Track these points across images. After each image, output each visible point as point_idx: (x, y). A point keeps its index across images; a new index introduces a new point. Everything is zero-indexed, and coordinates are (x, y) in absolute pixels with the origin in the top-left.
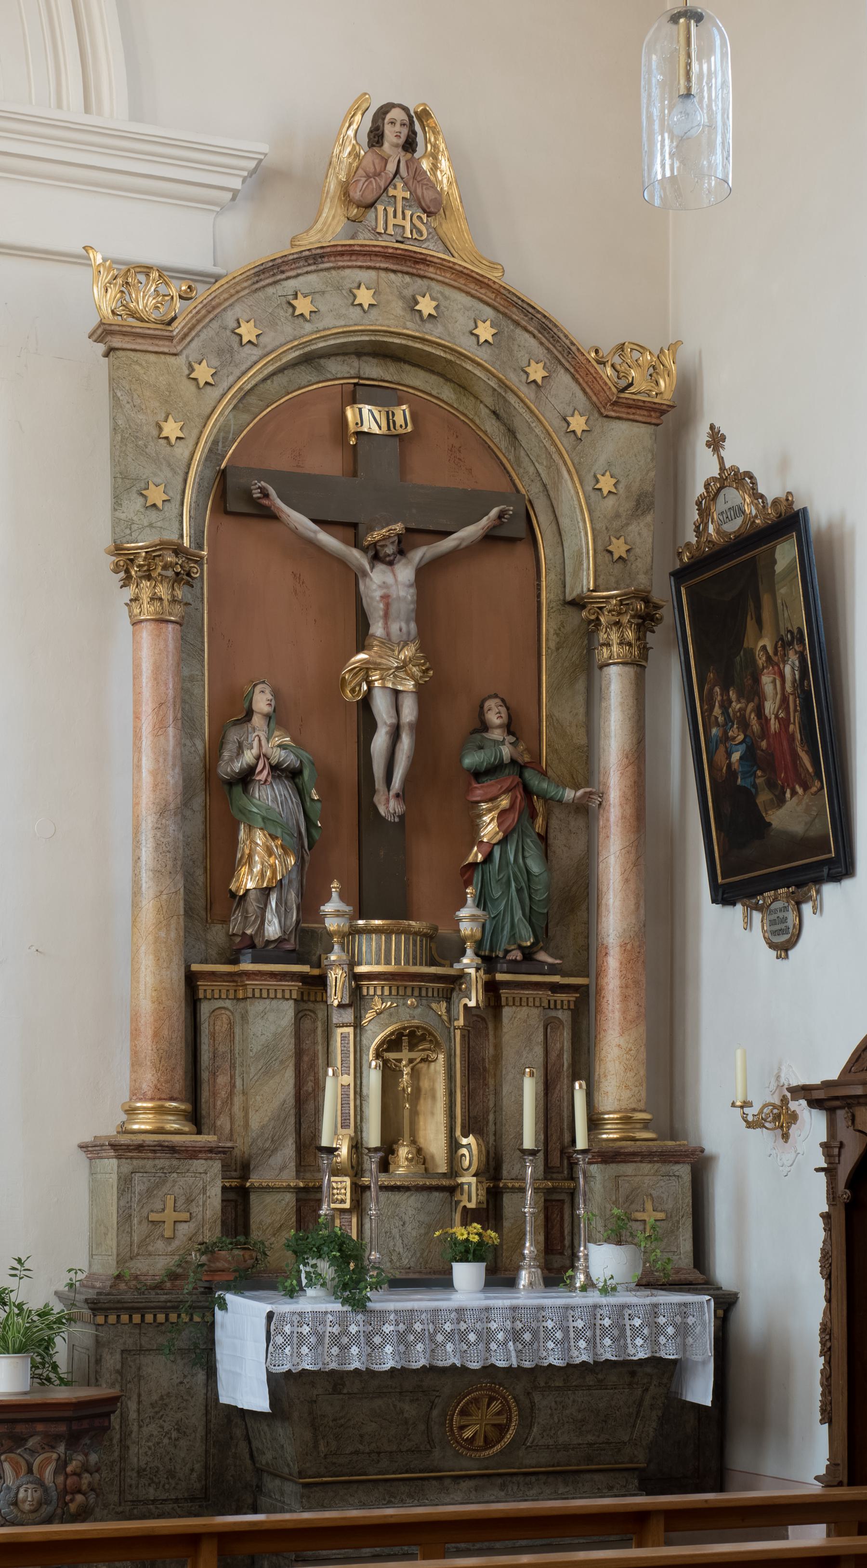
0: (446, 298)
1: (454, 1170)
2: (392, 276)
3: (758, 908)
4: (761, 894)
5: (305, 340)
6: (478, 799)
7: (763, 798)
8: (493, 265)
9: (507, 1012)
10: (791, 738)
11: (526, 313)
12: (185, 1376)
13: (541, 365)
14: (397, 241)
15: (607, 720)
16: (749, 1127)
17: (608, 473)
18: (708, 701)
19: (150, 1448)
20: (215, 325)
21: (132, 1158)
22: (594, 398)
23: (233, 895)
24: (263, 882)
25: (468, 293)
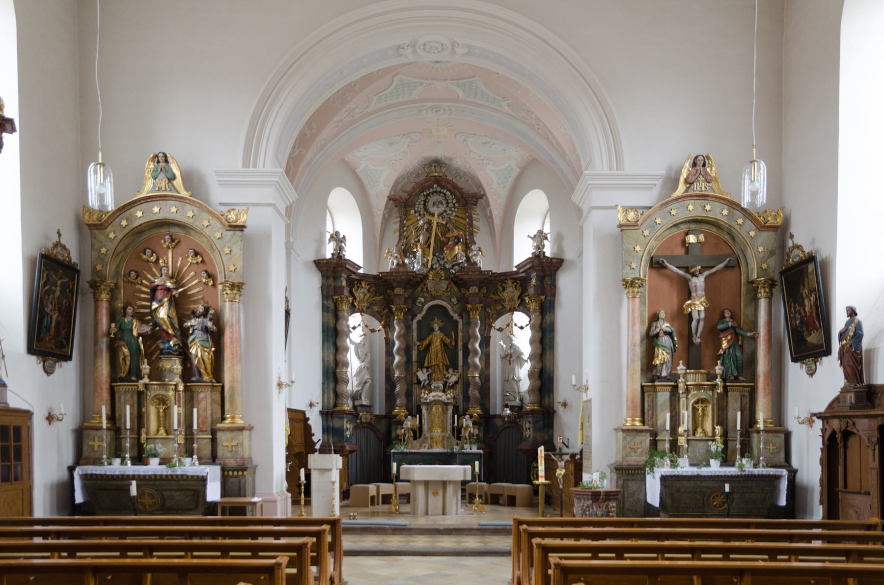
1: (714, 435)
3: (806, 364)
7: (805, 333)
9: (730, 393)
18: (790, 307)
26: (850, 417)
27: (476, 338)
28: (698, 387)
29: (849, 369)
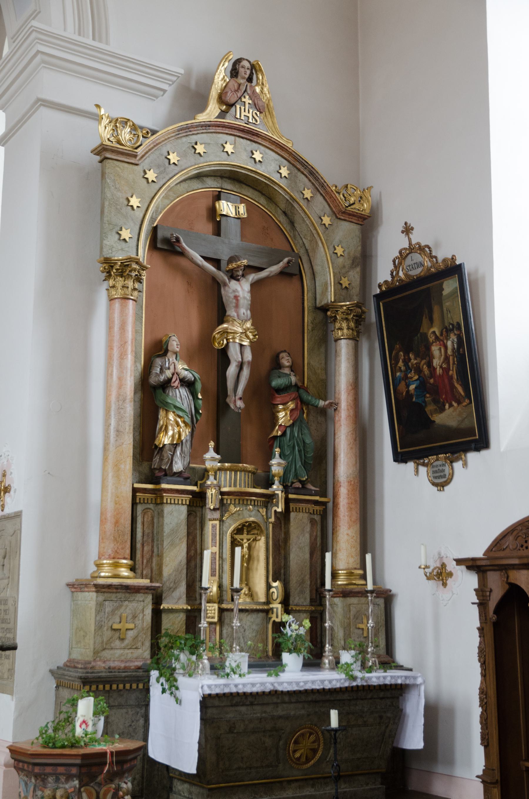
0: (266, 154)
3: (424, 465)
4: (427, 457)
5: (201, 165)
6: (279, 403)
7: (430, 408)
12: (133, 722)
13: (310, 191)
14: (245, 123)
15: (340, 367)
17: (340, 246)
21: (104, 592)
23: (156, 447)
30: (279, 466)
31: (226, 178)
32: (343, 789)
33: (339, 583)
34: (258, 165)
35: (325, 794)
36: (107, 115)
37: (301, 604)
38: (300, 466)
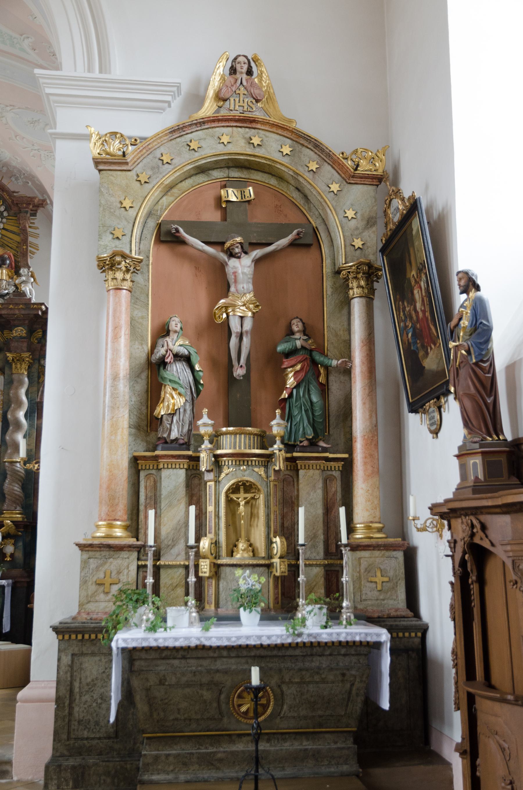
0: (267, 137)
1: (270, 556)
2: (239, 129)
7: (421, 354)
8: (290, 121)
9: (301, 472)
10: (427, 319)
11: (307, 140)
12: (106, 669)
16: (418, 531)
19: (85, 708)
20: (150, 156)
21: (88, 551)
22: (343, 175)
24: (168, 411)
25: (278, 134)
26: (476, 511)
27: (20, 404)
28: (240, 458)
29: (468, 404)
30: (279, 426)
31: (232, 167)
32: (305, 746)
33: (358, 536)
34: (230, 146)
35: (282, 750)
36: (96, 133)
37: (313, 558)
38: (307, 425)
